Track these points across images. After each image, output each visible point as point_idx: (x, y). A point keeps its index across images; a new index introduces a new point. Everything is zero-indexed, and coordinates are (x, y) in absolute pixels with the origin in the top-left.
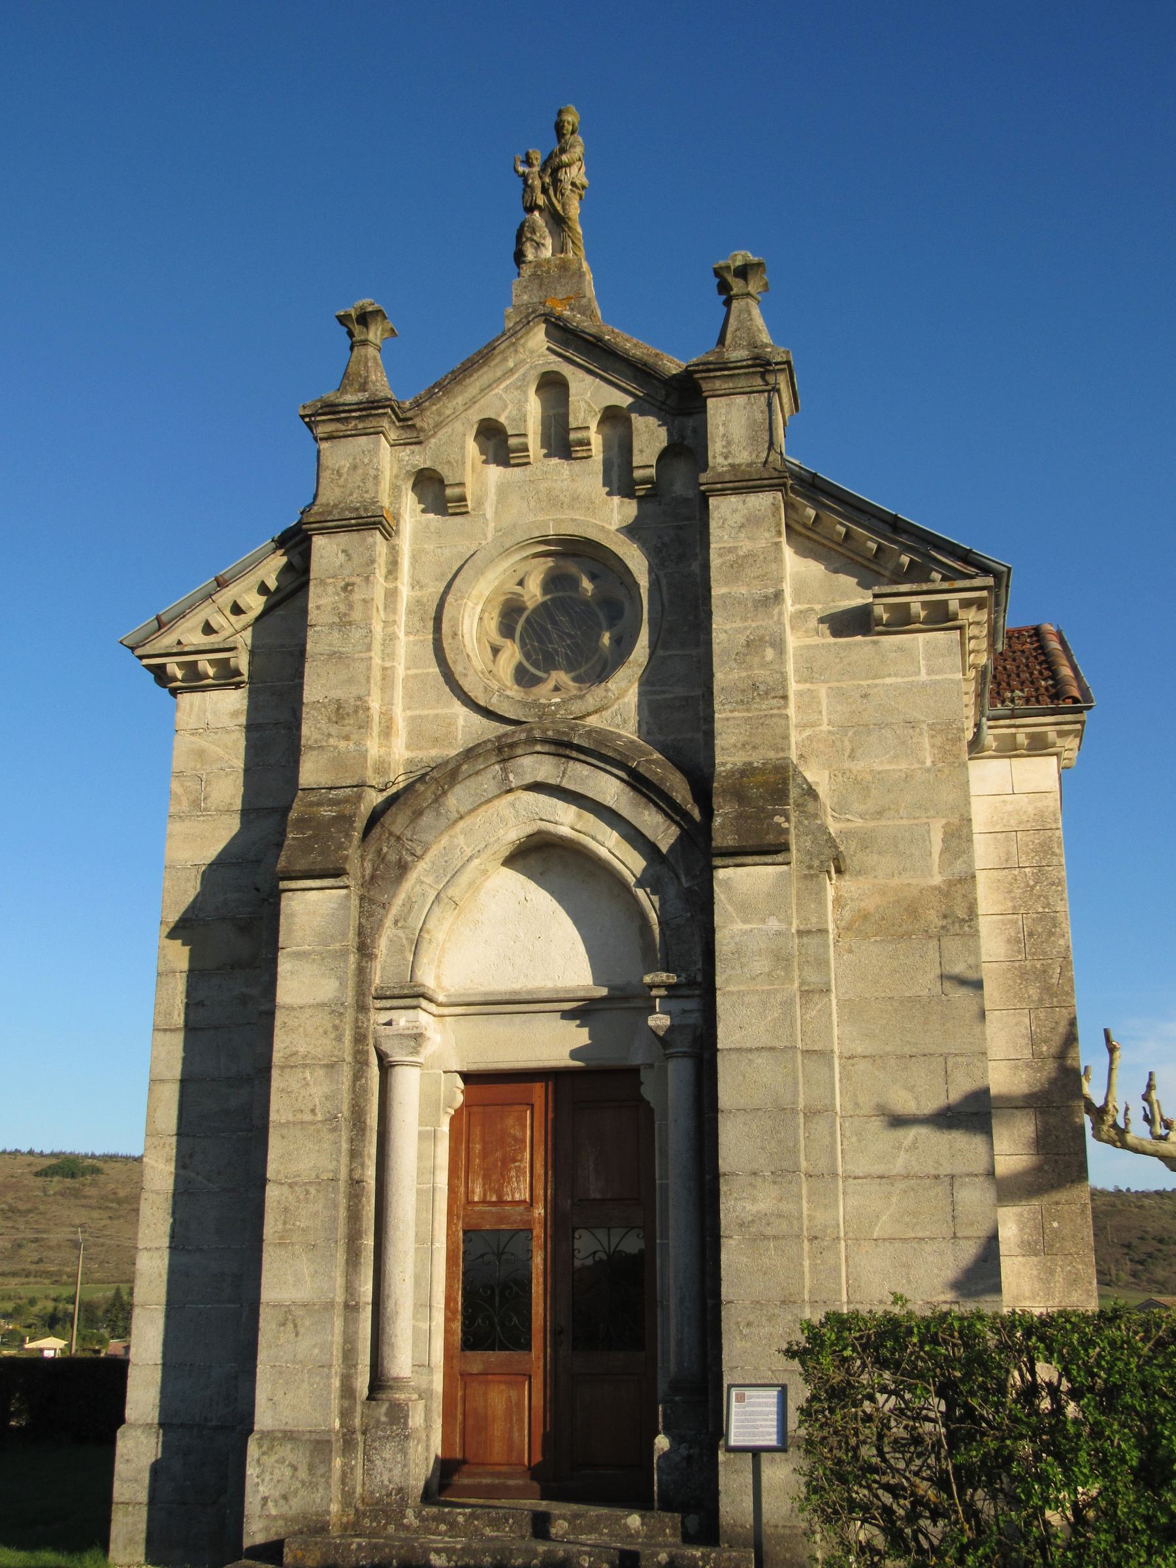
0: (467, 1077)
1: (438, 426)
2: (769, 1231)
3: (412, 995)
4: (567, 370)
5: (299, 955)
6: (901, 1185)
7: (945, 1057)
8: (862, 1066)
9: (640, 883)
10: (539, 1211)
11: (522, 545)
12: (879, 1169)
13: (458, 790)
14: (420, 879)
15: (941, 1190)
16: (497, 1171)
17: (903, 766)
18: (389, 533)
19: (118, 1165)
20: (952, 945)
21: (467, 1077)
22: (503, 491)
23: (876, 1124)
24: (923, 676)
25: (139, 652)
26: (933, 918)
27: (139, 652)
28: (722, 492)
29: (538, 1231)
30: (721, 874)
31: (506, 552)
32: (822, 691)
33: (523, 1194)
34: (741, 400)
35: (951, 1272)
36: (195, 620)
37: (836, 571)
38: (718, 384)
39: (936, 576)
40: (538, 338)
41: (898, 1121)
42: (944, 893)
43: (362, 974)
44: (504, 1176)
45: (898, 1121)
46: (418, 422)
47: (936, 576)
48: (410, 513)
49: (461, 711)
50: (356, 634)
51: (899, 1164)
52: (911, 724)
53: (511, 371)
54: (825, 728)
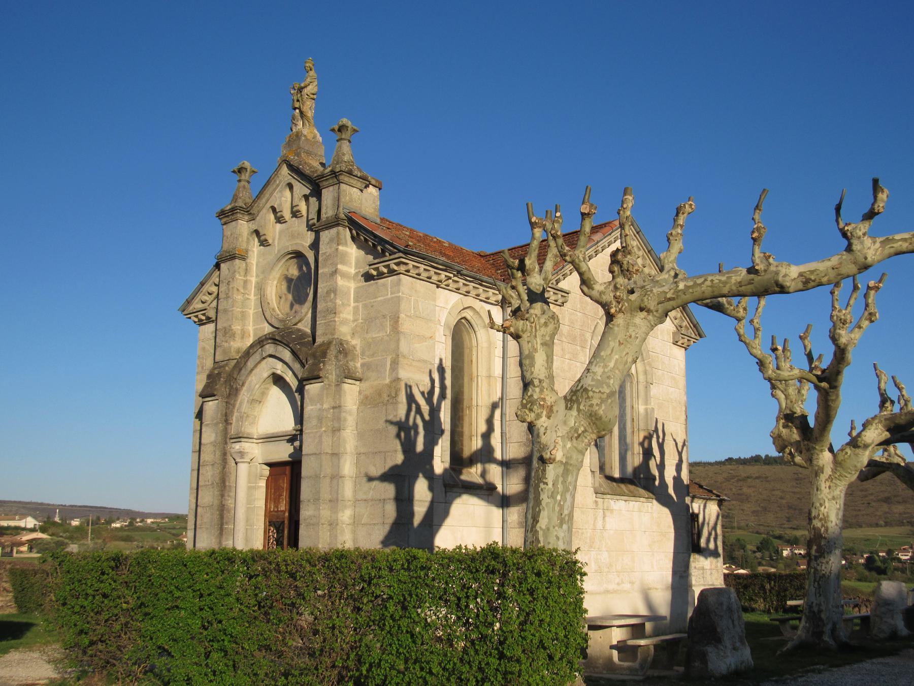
0: (270, 465)
1: (259, 212)
2: (312, 522)
3: (238, 438)
4: (294, 182)
5: (207, 425)
6: (370, 503)
7: (385, 452)
8: (363, 457)
9: (296, 391)
10: (287, 514)
11: (279, 260)
12: (364, 497)
13: (251, 359)
14: (244, 395)
15: (381, 505)
16: (277, 501)
17: (381, 335)
18: (243, 258)
19: (700, 468)
20: (390, 407)
21: (270, 465)
22: (281, 232)
23: (365, 479)
24: (389, 296)
25: (186, 312)
26: (385, 397)
27: (186, 312)
28: (322, 230)
29: (286, 522)
30: (307, 387)
31: (279, 260)
32: (360, 305)
33: (283, 508)
34: (331, 188)
35: (381, 538)
36: (197, 300)
37: (367, 254)
38: (324, 183)
39: (387, 254)
40: (285, 170)
41: (370, 479)
42: (389, 386)
43: (225, 431)
44: (279, 502)
45: (370, 479)
46: (252, 211)
47: (387, 254)
48: (255, 248)
49: (267, 325)
50: (230, 301)
51: (370, 497)
52: (384, 316)
53: (278, 185)
54: (360, 321)
